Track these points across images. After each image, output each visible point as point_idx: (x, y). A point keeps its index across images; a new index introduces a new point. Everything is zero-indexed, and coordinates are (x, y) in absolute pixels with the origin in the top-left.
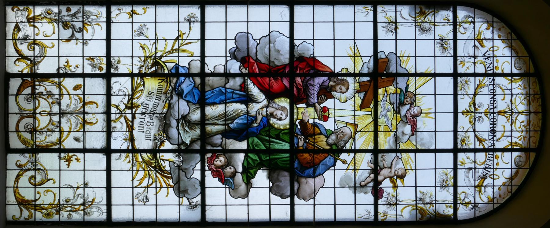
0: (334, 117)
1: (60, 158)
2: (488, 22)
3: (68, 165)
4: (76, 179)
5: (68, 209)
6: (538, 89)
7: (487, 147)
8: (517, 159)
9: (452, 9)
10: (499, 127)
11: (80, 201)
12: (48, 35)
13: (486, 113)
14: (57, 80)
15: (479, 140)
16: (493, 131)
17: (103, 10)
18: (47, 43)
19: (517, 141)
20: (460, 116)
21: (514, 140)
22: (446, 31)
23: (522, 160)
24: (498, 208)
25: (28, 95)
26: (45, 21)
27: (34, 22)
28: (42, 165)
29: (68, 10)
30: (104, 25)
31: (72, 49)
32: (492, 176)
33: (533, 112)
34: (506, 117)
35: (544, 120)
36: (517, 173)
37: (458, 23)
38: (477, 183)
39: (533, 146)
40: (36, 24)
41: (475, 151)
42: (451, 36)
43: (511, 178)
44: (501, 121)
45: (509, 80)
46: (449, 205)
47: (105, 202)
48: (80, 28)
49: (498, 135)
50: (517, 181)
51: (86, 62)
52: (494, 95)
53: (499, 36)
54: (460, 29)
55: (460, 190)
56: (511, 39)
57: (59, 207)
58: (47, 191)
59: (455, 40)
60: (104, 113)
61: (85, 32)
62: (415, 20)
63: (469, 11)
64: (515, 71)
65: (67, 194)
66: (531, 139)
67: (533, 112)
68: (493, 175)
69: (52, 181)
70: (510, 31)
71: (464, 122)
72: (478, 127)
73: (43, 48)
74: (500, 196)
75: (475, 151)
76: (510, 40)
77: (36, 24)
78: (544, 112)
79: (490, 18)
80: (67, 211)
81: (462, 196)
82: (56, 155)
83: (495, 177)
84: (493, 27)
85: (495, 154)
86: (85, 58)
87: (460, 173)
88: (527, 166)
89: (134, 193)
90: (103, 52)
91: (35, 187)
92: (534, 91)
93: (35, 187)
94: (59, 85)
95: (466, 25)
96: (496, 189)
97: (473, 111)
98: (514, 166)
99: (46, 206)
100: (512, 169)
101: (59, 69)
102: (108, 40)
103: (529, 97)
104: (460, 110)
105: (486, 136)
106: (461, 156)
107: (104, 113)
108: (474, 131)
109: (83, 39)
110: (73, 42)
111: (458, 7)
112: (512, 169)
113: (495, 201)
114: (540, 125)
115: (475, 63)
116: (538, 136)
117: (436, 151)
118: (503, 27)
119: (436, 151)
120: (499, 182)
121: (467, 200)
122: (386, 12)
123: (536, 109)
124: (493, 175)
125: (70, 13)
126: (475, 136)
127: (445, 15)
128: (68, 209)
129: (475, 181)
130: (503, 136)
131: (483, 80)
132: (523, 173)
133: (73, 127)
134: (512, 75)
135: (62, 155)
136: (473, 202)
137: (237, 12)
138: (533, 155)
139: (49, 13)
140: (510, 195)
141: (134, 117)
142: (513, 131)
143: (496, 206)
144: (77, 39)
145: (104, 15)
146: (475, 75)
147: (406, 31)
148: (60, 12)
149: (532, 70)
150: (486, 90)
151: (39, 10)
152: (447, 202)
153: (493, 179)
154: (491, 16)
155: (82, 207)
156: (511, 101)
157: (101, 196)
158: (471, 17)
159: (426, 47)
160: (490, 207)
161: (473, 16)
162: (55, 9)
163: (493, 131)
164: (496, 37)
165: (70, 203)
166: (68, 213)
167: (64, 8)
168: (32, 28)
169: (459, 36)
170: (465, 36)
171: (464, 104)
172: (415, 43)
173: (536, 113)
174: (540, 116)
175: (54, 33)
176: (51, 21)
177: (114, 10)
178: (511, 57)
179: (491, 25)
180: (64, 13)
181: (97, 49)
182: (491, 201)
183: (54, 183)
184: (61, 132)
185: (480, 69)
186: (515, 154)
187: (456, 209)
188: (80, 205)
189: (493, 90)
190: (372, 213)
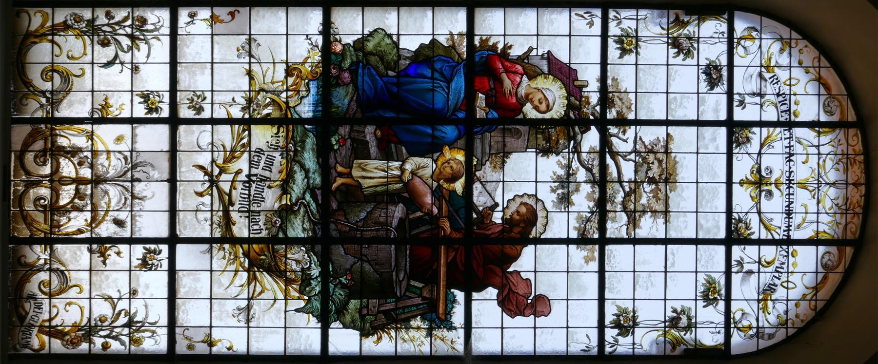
0: (819, 154)
1: (91, 251)
2: (781, 39)
3: (104, 263)
4: (116, 283)
5: (102, 333)
6: (859, 147)
7: (777, 237)
8: (826, 258)
9: (726, 16)
10: (797, 207)
11: (123, 320)
12: (76, 55)
13: (777, 184)
14: (88, 127)
15: (766, 227)
16: (789, 213)
17: (164, 14)
18: (74, 69)
19: (826, 228)
20: (736, 188)
21: (822, 228)
22: (713, 51)
23: (832, 258)
24: (794, 335)
25: (39, 151)
26: (70, 33)
27: (53, 35)
28: (62, 264)
29: (109, 15)
30: (166, 40)
31: (116, 79)
32: (785, 284)
33: (853, 184)
34: (811, 192)
35: (868, 196)
36: (825, 278)
37: (736, 40)
38: (761, 297)
39: (849, 236)
40: (56, 38)
41: (760, 242)
42: (724, 61)
43: (816, 289)
44: (802, 197)
45: (816, 131)
46: (718, 330)
47: (164, 321)
48: (128, 46)
49: (797, 219)
50: (825, 293)
51: (137, 99)
52: (791, 155)
53: (800, 63)
54: (739, 51)
55: (734, 306)
56: (819, 67)
57: (89, 331)
58: (69, 304)
59: (731, 65)
60: (168, 181)
61: (135, 51)
62: (668, 34)
63: (751, 22)
64: (824, 118)
65: (102, 309)
66: (849, 227)
67: (853, 184)
68: (788, 281)
69: (77, 289)
70: (817, 53)
71: (743, 198)
72: (765, 205)
73: (66, 77)
74: (797, 316)
75: (760, 242)
76: (817, 69)
77: (56, 38)
78: (869, 184)
79: (785, 32)
80: (101, 336)
81: (738, 316)
82: (84, 247)
83: (791, 285)
84: (790, 47)
85: (791, 249)
86: (134, 93)
87: (736, 278)
88: (841, 269)
89: (217, 301)
90: (163, 84)
91: (50, 299)
92: (854, 150)
93: (50, 299)
94: (91, 136)
95: (748, 43)
96: (791, 304)
97: (759, 182)
98: (820, 269)
99: (67, 329)
100: (817, 272)
101: (93, 111)
102: (174, 63)
103: (845, 160)
104: (736, 178)
105: (779, 221)
106: (736, 250)
107: (168, 181)
108: (759, 213)
109: (132, 63)
110: (117, 67)
111: (736, 13)
112: (817, 272)
113: (790, 325)
114: (862, 204)
115: (761, 105)
116: (857, 221)
117: (696, 242)
118: (806, 46)
119: (696, 242)
120: (795, 294)
121: (745, 323)
122: (625, 20)
123: (856, 178)
124: (788, 281)
125: (111, 22)
126: (761, 220)
127: (713, 27)
128: (102, 333)
129: (758, 293)
130: (804, 220)
131: (773, 132)
132: (835, 279)
133: (113, 203)
134: (210, 241)
135: (95, 246)
136: (754, 324)
137: (442, 349)
138: (849, 251)
139: (78, 19)
140: (813, 314)
141: (233, 187)
142: (816, 211)
143: (791, 332)
144: (122, 63)
145: (167, 23)
146: (761, 124)
147: (654, 51)
148: (93, 20)
149: (852, 117)
150: (779, 146)
151: (61, 15)
152: (714, 325)
153: (787, 288)
154: (788, 29)
155: (126, 331)
156: (819, 164)
157: (159, 312)
158: (757, 30)
159: (687, 76)
160: (781, 335)
161: (759, 29)
162: (87, 14)
163: (789, 213)
164: (795, 63)
165: (106, 323)
166: (103, 340)
167: (101, 13)
168: (49, 45)
169: (737, 61)
170: (746, 61)
171: (743, 167)
172: (660, 74)
173: (856, 185)
174: (863, 189)
175: (85, 54)
176: (80, 34)
177: (184, 15)
178: (819, 95)
179: (786, 44)
180: (102, 20)
181: (156, 78)
182: (783, 324)
183: (81, 292)
184: (94, 210)
185: (771, 114)
186: (822, 249)
187: (728, 336)
188: (124, 326)
189: (790, 147)
190: (595, 342)
